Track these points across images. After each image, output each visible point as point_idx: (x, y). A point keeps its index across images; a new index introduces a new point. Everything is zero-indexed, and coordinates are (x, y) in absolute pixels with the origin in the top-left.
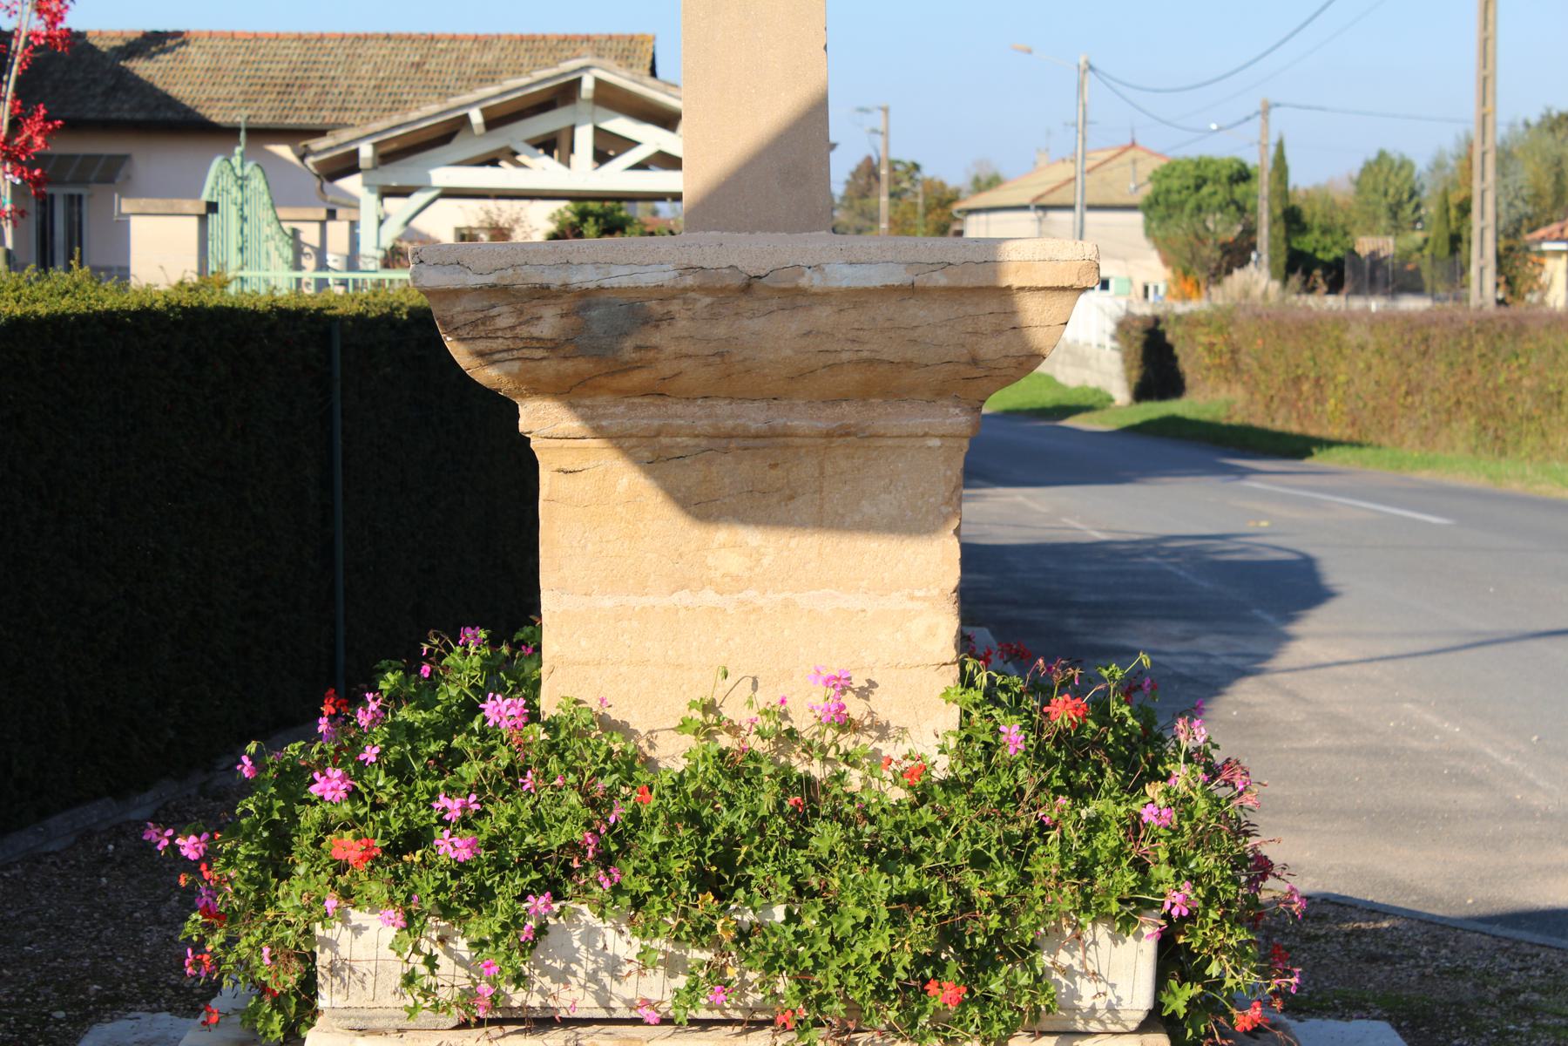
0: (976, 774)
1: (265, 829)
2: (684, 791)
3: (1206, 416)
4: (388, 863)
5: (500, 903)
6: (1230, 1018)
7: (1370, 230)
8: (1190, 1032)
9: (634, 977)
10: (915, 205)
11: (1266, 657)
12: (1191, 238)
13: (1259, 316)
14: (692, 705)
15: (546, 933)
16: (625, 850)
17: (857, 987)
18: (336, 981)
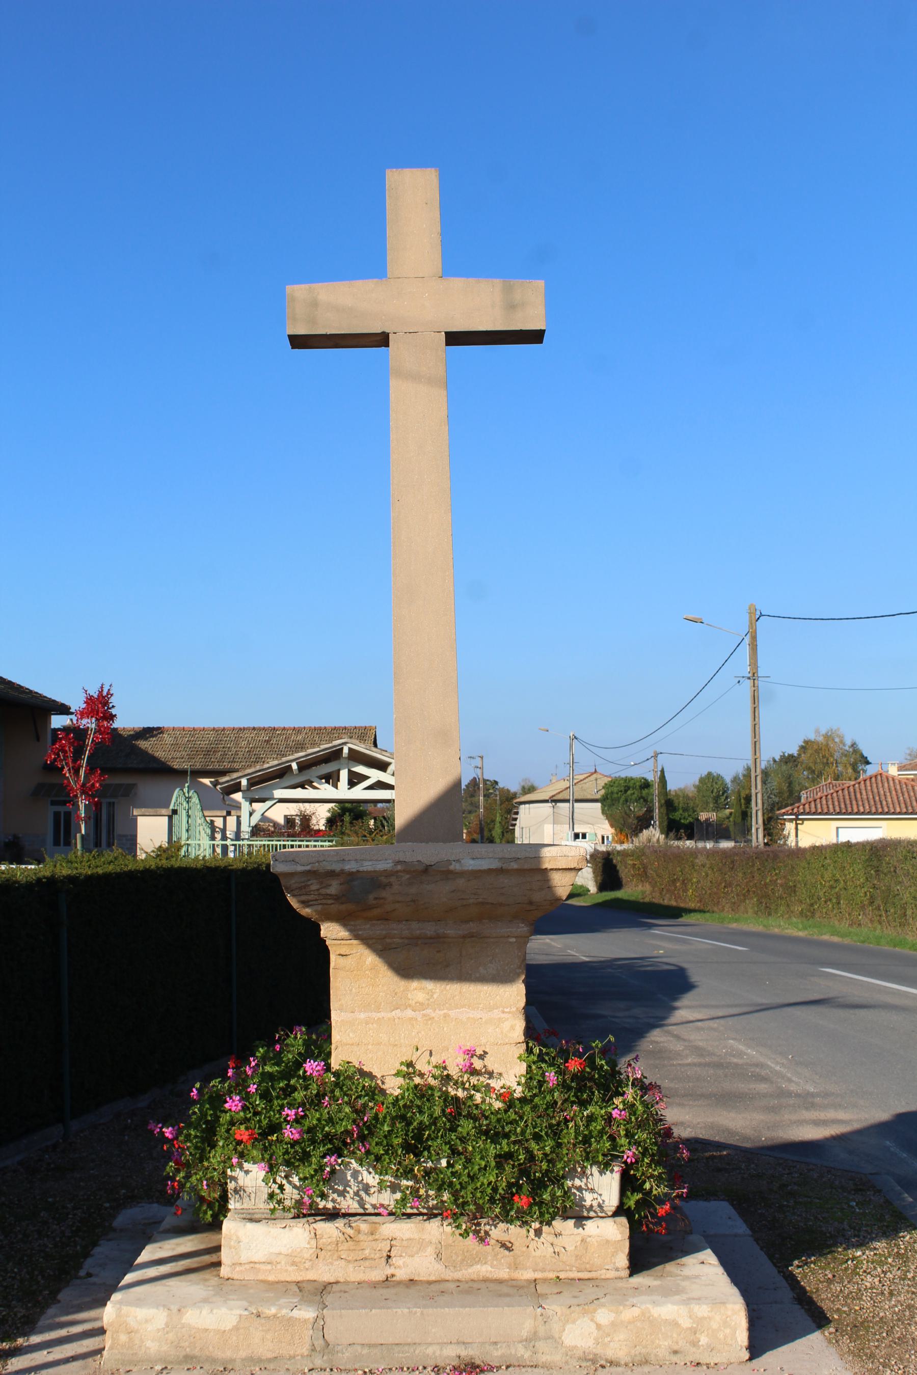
0: (535, 1094)
1: (204, 1123)
2: (399, 1105)
3: (633, 898)
4: (261, 1140)
5: (314, 1160)
6: (655, 1209)
7: (705, 809)
8: (637, 1216)
9: (376, 1194)
10: (496, 800)
11: (665, 1018)
12: (623, 814)
13: (656, 852)
14: (402, 1063)
15: (335, 1173)
16: (371, 1133)
17: (481, 1198)
18: (237, 1196)
